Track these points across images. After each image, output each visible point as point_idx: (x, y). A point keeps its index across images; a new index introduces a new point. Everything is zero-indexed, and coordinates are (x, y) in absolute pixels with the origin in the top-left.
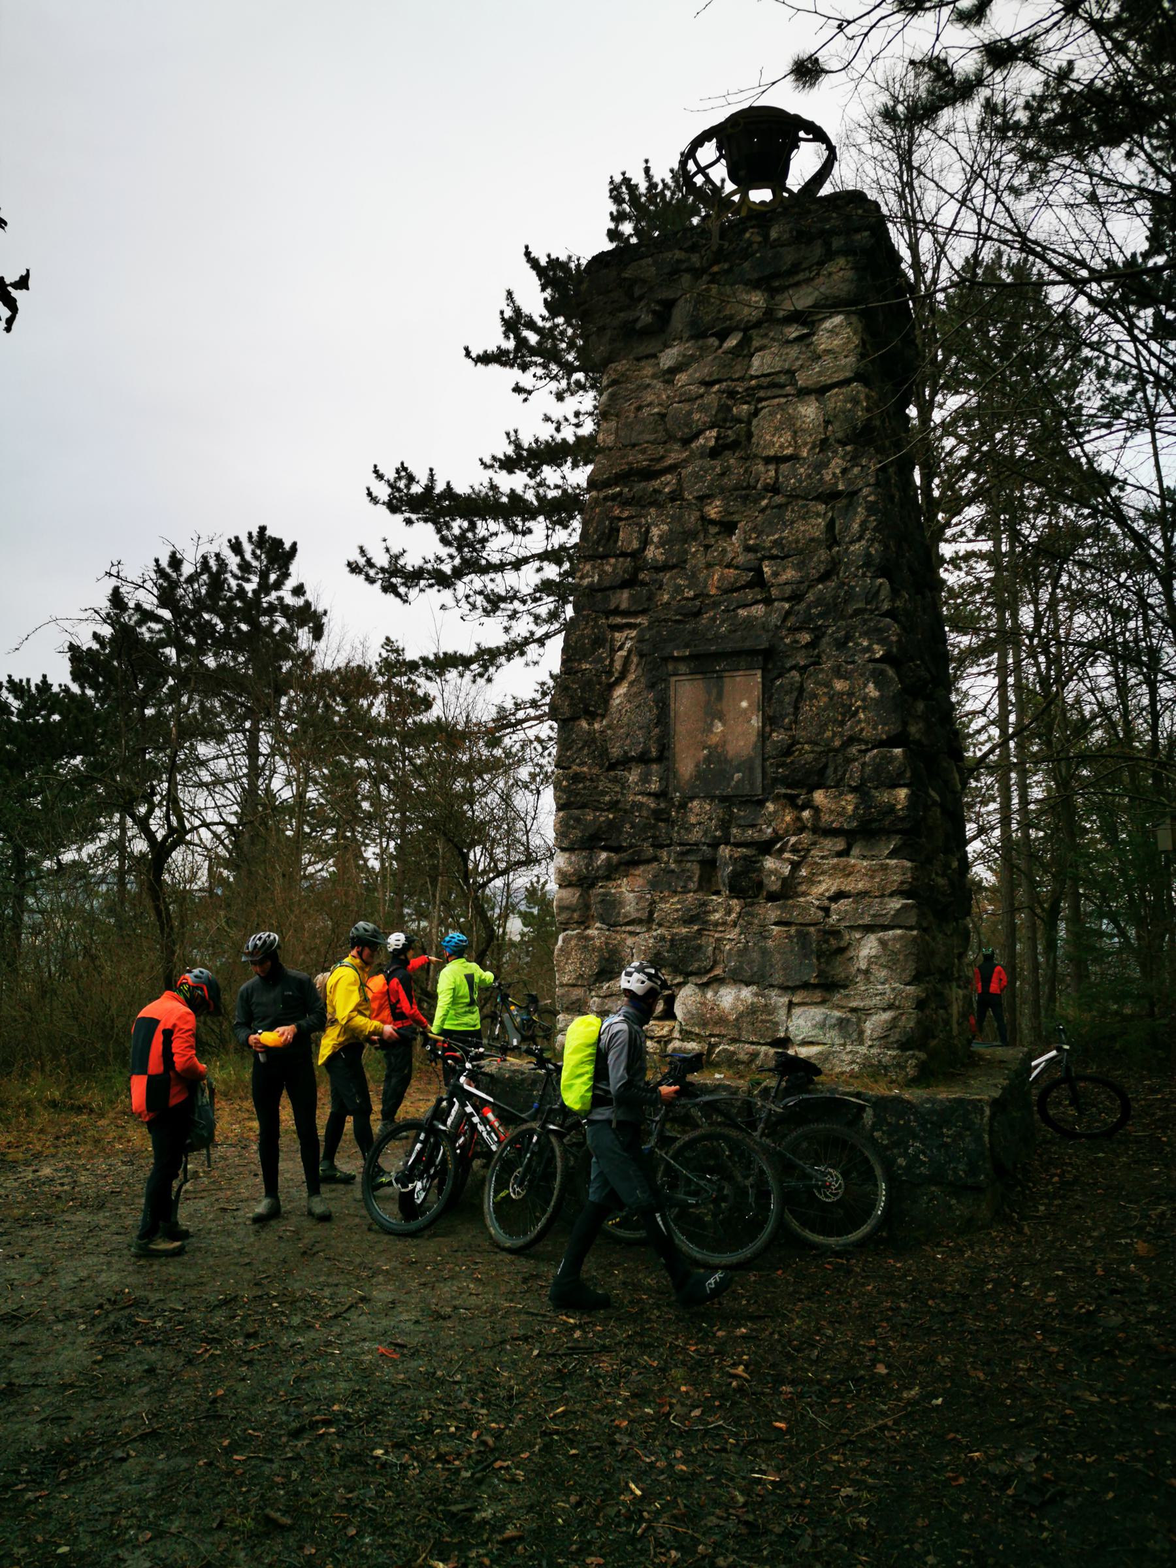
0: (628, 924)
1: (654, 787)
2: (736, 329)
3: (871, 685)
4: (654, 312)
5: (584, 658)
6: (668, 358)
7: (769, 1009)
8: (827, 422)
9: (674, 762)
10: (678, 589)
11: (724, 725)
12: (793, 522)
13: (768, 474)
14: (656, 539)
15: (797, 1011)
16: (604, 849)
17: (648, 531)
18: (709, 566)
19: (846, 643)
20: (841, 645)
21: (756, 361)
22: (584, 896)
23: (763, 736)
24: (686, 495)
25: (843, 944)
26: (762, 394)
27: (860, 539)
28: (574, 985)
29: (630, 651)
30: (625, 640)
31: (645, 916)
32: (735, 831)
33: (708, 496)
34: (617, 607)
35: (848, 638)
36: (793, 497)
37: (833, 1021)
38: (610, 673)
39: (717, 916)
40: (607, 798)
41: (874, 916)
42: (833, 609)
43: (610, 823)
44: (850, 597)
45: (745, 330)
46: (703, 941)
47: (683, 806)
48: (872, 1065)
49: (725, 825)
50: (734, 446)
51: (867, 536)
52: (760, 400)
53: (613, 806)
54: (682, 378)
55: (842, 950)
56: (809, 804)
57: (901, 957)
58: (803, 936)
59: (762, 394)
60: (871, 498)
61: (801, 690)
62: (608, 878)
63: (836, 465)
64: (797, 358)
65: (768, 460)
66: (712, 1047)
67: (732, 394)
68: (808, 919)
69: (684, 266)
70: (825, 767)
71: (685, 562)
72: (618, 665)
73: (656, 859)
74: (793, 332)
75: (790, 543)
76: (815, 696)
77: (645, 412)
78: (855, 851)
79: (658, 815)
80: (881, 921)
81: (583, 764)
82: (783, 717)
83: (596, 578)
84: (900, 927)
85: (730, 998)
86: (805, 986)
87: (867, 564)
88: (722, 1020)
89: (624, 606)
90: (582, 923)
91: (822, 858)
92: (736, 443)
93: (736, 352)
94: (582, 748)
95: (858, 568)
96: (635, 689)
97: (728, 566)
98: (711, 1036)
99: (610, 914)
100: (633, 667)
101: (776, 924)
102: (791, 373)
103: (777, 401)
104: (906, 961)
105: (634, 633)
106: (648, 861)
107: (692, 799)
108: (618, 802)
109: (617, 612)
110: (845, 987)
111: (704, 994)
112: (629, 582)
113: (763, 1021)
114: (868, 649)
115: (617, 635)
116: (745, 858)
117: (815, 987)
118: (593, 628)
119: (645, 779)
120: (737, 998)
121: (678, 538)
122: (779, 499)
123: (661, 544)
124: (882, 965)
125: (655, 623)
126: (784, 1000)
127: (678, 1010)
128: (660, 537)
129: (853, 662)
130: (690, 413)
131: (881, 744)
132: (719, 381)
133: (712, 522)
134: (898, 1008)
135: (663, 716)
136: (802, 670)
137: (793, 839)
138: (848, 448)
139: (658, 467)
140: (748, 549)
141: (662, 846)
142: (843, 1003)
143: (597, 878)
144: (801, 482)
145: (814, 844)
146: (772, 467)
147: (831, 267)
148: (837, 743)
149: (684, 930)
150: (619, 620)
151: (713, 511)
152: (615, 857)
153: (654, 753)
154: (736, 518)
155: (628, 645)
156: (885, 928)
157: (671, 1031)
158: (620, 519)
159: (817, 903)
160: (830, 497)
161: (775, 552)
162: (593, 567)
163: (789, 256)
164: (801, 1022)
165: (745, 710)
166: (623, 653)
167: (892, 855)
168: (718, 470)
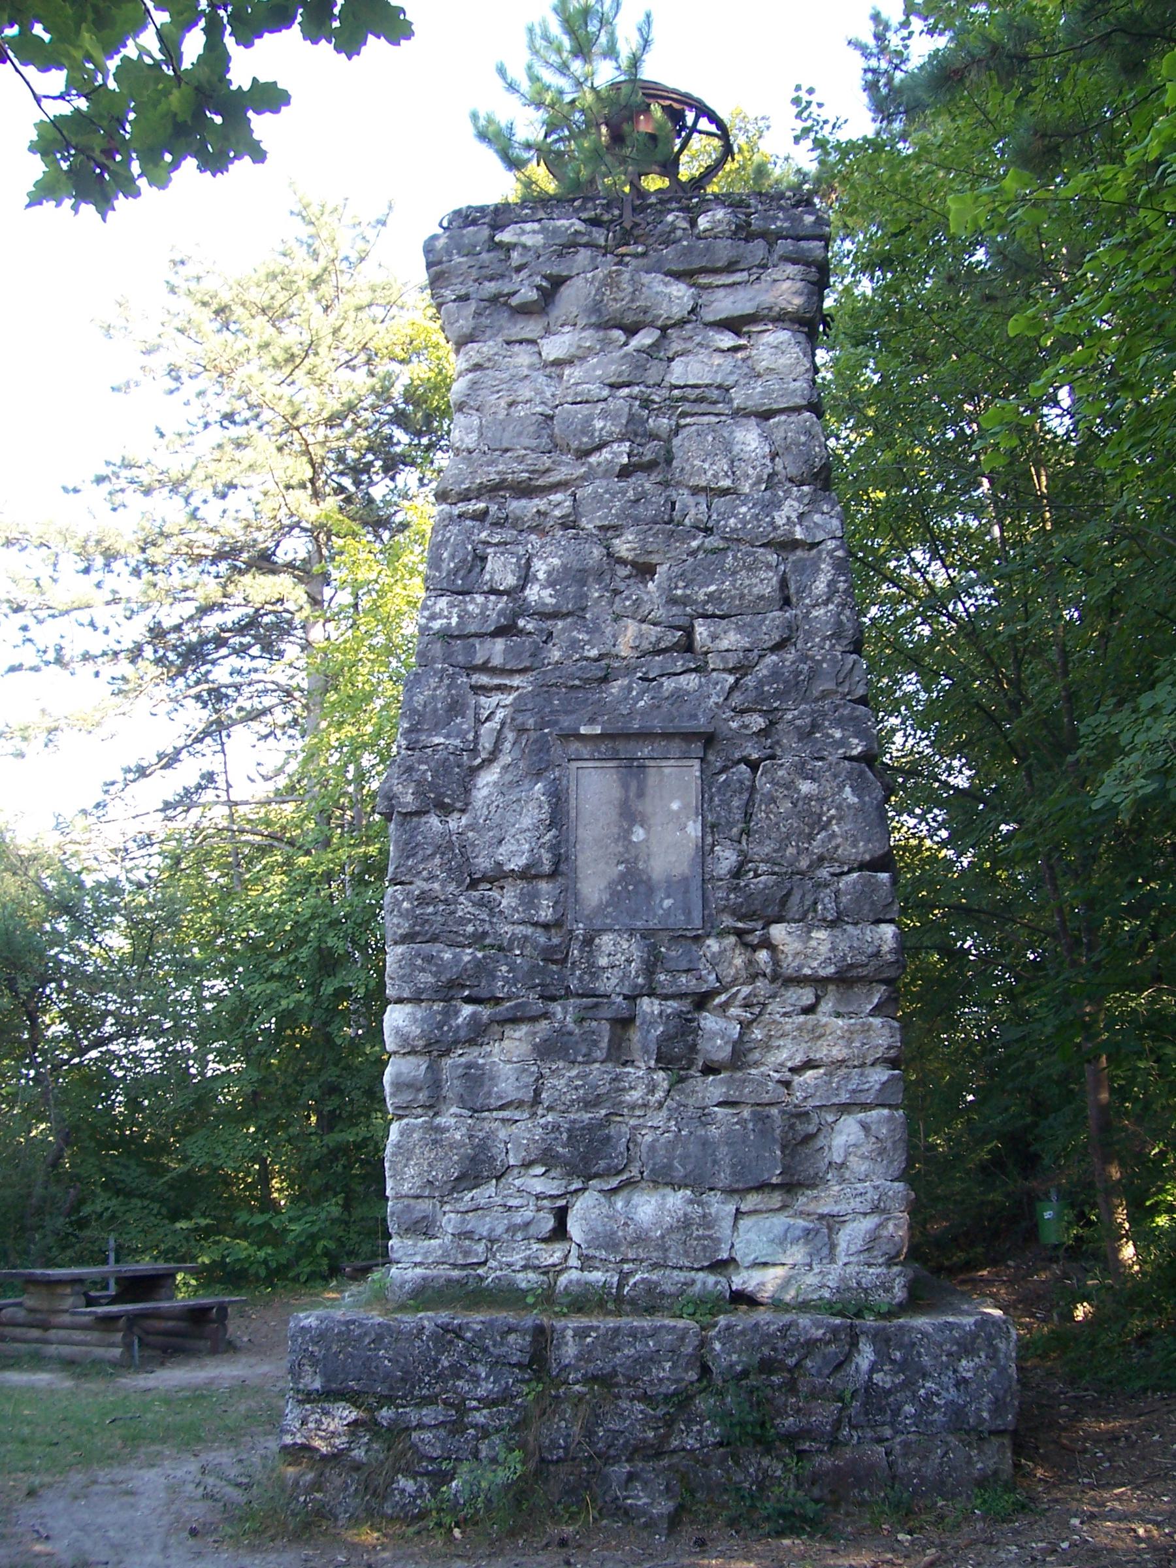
0: (501, 1108)
1: (546, 913)
2: (651, 325)
3: (848, 789)
4: (538, 288)
5: (435, 729)
6: (554, 348)
7: (707, 1221)
8: (774, 456)
9: (576, 880)
10: (574, 644)
11: (648, 832)
12: (734, 573)
13: (694, 510)
14: (541, 576)
15: (744, 1223)
16: (469, 1000)
17: (528, 565)
18: (617, 618)
19: (811, 733)
20: (805, 735)
21: (677, 366)
22: (433, 1068)
23: (705, 852)
24: (584, 522)
25: (812, 1129)
26: (686, 407)
27: (826, 603)
28: (418, 1197)
29: (503, 724)
30: (497, 707)
31: (528, 1095)
32: (662, 977)
33: (614, 528)
34: (487, 661)
35: (815, 727)
36: (733, 540)
37: (798, 1233)
38: (474, 752)
39: (635, 1095)
40: (470, 929)
41: (854, 1091)
42: (794, 686)
43: (478, 964)
44: (814, 674)
45: (664, 329)
46: (613, 1130)
47: (588, 942)
48: (849, 1289)
49: (651, 966)
50: (650, 467)
51: (837, 600)
52: (684, 415)
53: (478, 939)
54: (572, 374)
55: (809, 1138)
56: (767, 943)
57: (889, 1145)
58: (761, 1119)
59: (686, 407)
60: (840, 553)
61: (753, 789)
62: (471, 1042)
63: (789, 509)
64: (731, 373)
65: (696, 491)
66: (624, 1277)
67: (646, 403)
68: (766, 1098)
69: (585, 239)
70: (789, 894)
71: (584, 609)
72: (486, 743)
73: (546, 1015)
74: (727, 340)
75: (732, 598)
76: (773, 800)
77: (521, 411)
78: (826, 1006)
79: (550, 955)
80: (862, 1098)
81: (432, 878)
82: (730, 825)
83: (454, 621)
84: (883, 1106)
85: (650, 1208)
86: (762, 1187)
87: (837, 635)
88: (640, 1239)
89: (497, 661)
90: (431, 1107)
91: (785, 1015)
92: (652, 462)
93: (649, 352)
94: (433, 855)
95: (824, 639)
96: (508, 777)
97: (643, 621)
98: (623, 1261)
99: (475, 1090)
100: (507, 745)
101: (719, 1105)
102: (724, 389)
103: (706, 419)
104: (895, 1149)
105: (509, 699)
106: (533, 1019)
107: (600, 931)
108: (485, 934)
109: (485, 668)
110: (813, 1186)
111: (612, 1205)
112: (505, 630)
113: (698, 1238)
114: (842, 743)
115: (483, 699)
116: (679, 1014)
117: (774, 1187)
118: (449, 687)
119: (529, 900)
120: (661, 1207)
121: (573, 577)
122: (713, 542)
123: (551, 583)
124: (863, 1157)
125: (545, 689)
126: (731, 1208)
127: (575, 1228)
128: (549, 573)
129: (822, 759)
130: (589, 419)
131: (862, 867)
132: (628, 385)
133: (622, 561)
134: (884, 1211)
135: (559, 814)
136: (754, 766)
137: (746, 990)
138: (806, 488)
139: (540, 482)
140: (673, 601)
141: (553, 999)
142: (811, 1207)
143: (456, 1042)
144: (745, 524)
145: (773, 996)
146: (702, 499)
147: (773, 273)
148: (804, 864)
149: (587, 1116)
150: (484, 679)
151: (624, 546)
152: (485, 1012)
153: (547, 868)
154: (654, 559)
155: (500, 714)
156: (865, 1107)
157: (566, 1257)
158: (487, 544)
159: (776, 1076)
160: (788, 545)
161: (710, 608)
162: (451, 605)
163: (724, 250)
164: (752, 1236)
165: (677, 814)
166: (494, 724)
167: (874, 1013)
168: (630, 494)
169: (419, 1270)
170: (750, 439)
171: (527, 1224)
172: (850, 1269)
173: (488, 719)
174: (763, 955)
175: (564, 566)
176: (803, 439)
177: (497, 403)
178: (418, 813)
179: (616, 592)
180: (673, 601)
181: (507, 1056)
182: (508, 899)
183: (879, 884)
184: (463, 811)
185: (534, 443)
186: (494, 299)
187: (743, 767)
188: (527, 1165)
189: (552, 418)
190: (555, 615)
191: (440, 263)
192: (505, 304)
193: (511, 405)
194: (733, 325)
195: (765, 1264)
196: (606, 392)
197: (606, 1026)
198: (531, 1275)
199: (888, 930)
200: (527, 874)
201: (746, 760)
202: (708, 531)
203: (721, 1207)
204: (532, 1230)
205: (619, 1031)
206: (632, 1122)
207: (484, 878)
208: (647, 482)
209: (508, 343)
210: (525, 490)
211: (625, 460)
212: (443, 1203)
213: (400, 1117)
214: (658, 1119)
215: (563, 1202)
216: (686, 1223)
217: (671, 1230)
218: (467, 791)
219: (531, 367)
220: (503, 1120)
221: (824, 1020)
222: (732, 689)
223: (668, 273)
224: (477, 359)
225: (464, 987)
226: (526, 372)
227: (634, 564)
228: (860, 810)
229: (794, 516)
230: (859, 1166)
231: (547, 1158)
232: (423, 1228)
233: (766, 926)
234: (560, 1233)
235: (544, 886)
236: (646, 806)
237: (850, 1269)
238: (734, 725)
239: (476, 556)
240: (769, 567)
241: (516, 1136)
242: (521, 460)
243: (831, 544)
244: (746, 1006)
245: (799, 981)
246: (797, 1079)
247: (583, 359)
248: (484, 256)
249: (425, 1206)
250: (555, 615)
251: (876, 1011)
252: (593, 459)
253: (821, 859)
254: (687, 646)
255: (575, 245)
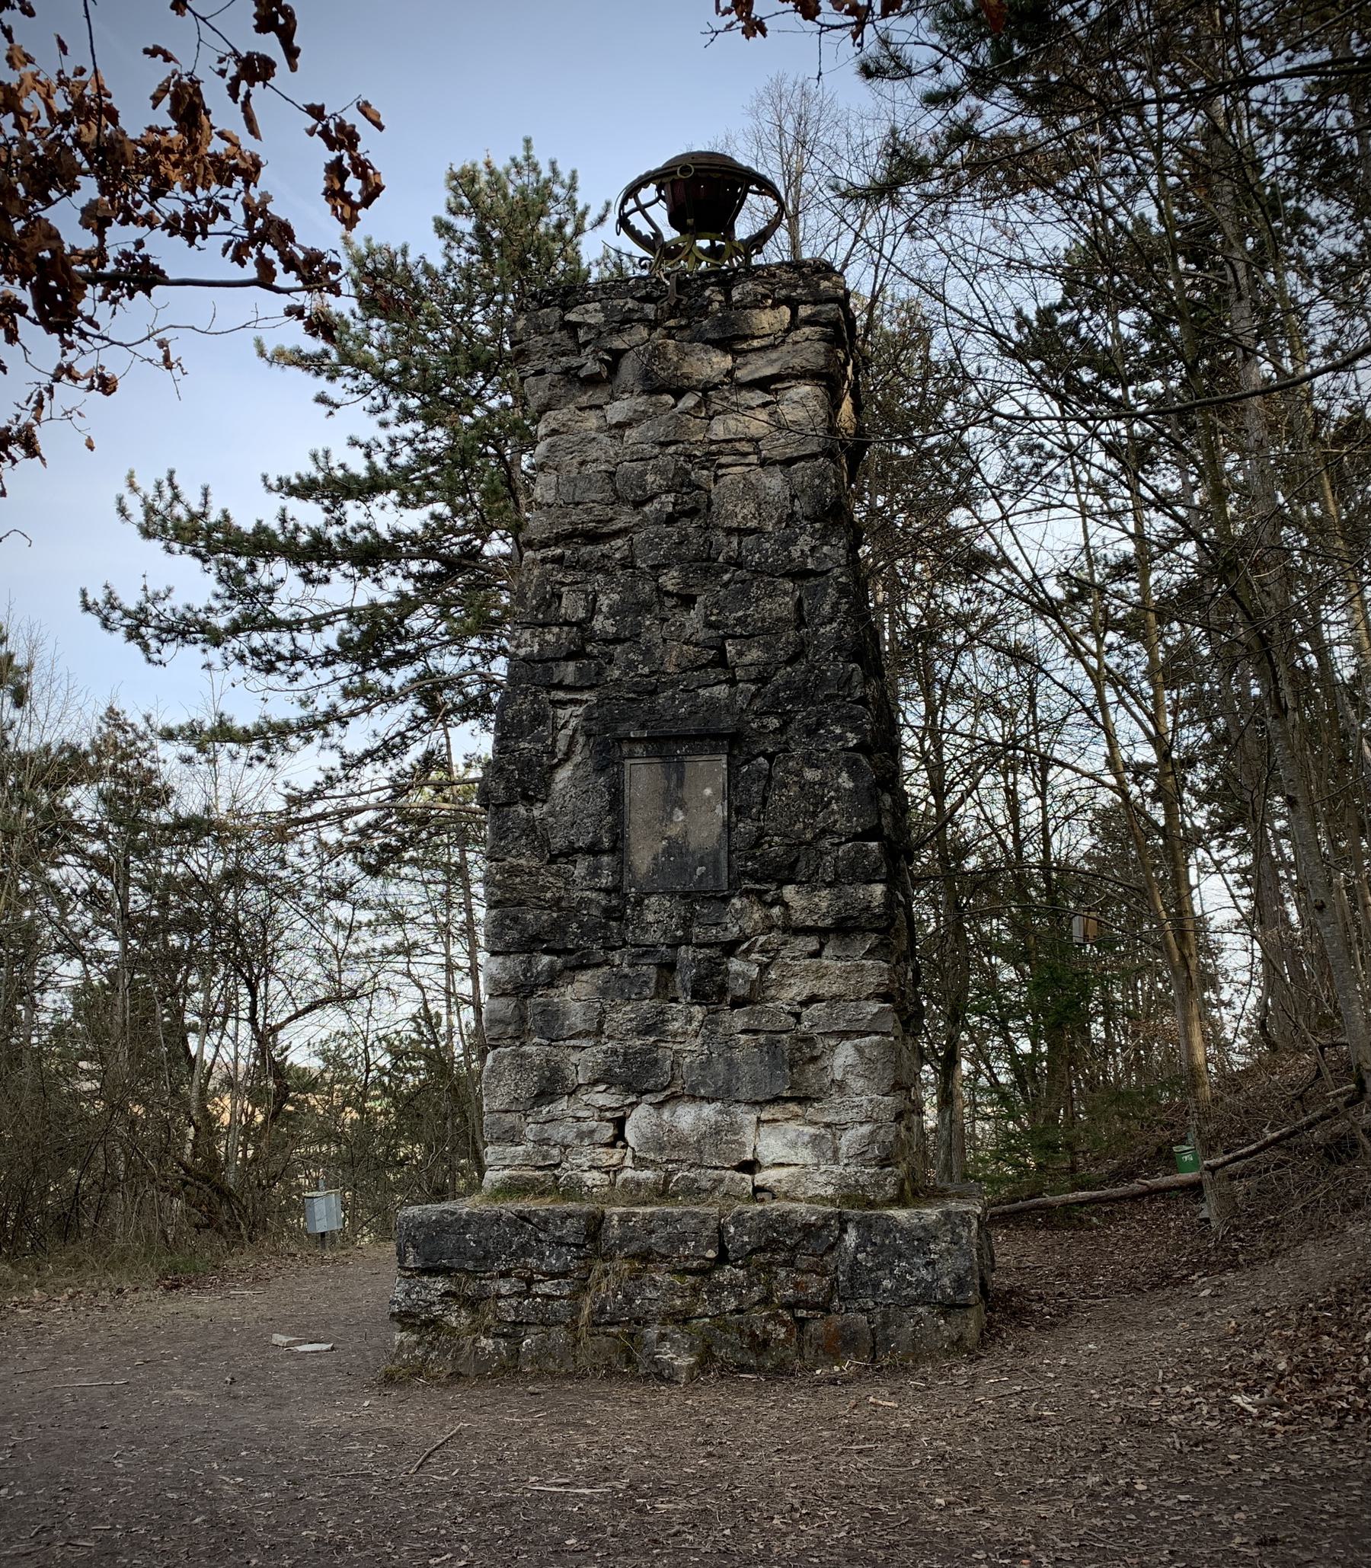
0: (571, 1038)
1: (605, 881)
3: (844, 775)
6: (617, 411)
8: (793, 497)
10: (631, 665)
12: (758, 600)
14: (604, 609)
16: (546, 952)
17: (595, 600)
23: (729, 827)
24: (639, 563)
27: (831, 621)
29: (575, 730)
30: (570, 717)
35: (820, 724)
38: (553, 754)
39: (675, 1026)
40: (549, 895)
42: (802, 694)
45: (705, 391)
47: (639, 902)
54: (632, 434)
61: (769, 778)
62: (550, 985)
63: (805, 542)
65: (730, 532)
70: (797, 860)
71: (638, 635)
72: (562, 746)
74: (757, 397)
77: (590, 469)
80: (856, 1027)
81: (520, 855)
83: (536, 648)
84: (877, 1033)
85: (687, 1117)
88: (681, 1144)
92: (693, 506)
96: (580, 773)
99: (551, 1024)
100: (579, 747)
101: (743, 1032)
105: (580, 710)
106: (598, 965)
107: (649, 895)
108: (561, 898)
109: (559, 686)
110: (819, 1100)
111: (659, 1116)
114: (841, 737)
115: (560, 712)
118: (532, 703)
121: (631, 608)
126: (753, 1117)
128: (610, 607)
131: (857, 837)
133: (669, 594)
135: (616, 801)
136: (770, 758)
137: (762, 939)
138: (817, 525)
141: (614, 948)
145: (785, 943)
148: (809, 836)
150: (561, 695)
152: (559, 962)
153: (606, 843)
154: (695, 591)
155: (573, 723)
158: (563, 584)
160: (800, 575)
161: (738, 630)
162: (533, 635)
169: (507, 1172)
170: (774, 482)
171: (592, 1132)
172: (851, 1170)
173: (564, 726)
174: (776, 911)
175: (622, 600)
176: (817, 481)
177: (571, 462)
178: (508, 804)
179: (664, 620)
180: (709, 625)
181: (575, 997)
182: (580, 870)
183: (867, 854)
184: (544, 802)
185: (600, 496)
186: (566, 371)
187: (761, 759)
188: (595, 1083)
189: (613, 474)
190: (617, 640)
191: (521, 341)
192: (576, 375)
193: (582, 463)
194: (762, 384)
195: (782, 1165)
196: (657, 450)
197: (652, 971)
198: (595, 1174)
199: (879, 889)
200: (594, 850)
201: (763, 754)
202: (739, 566)
203: (747, 1117)
204: (597, 1137)
205: (665, 973)
206: (676, 1047)
207: (561, 854)
208: (690, 527)
209: (581, 409)
210: (593, 537)
211: (670, 509)
212: (526, 1116)
213: (495, 1047)
214: (695, 1044)
215: (619, 1114)
216: (717, 1130)
217: (703, 1136)
218: (548, 786)
219: (599, 430)
220: (574, 1047)
221: (826, 962)
222: (754, 696)
223: (707, 342)
224: (554, 425)
225: (544, 941)
226: (593, 434)
227: (677, 595)
228: (854, 792)
229: (806, 549)
230: (856, 1084)
231: (605, 1078)
232: (512, 1137)
233: (779, 888)
234: (620, 1135)
235: (605, 859)
236: (686, 793)
237: (851, 1170)
238: (754, 726)
239: (553, 595)
240: (786, 593)
241: (582, 1061)
242: (589, 511)
243: (837, 571)
244: (763, 951)
245: (807, 931)
246: (805, 1012)
247: (639, 421)
248: (557, 335)
249: (511, 1119)
250: (617, 640)
251: (870, 953)
252: (646, 509)
253: (824, 831)
254: (721, 661)
255: (630, 321)
